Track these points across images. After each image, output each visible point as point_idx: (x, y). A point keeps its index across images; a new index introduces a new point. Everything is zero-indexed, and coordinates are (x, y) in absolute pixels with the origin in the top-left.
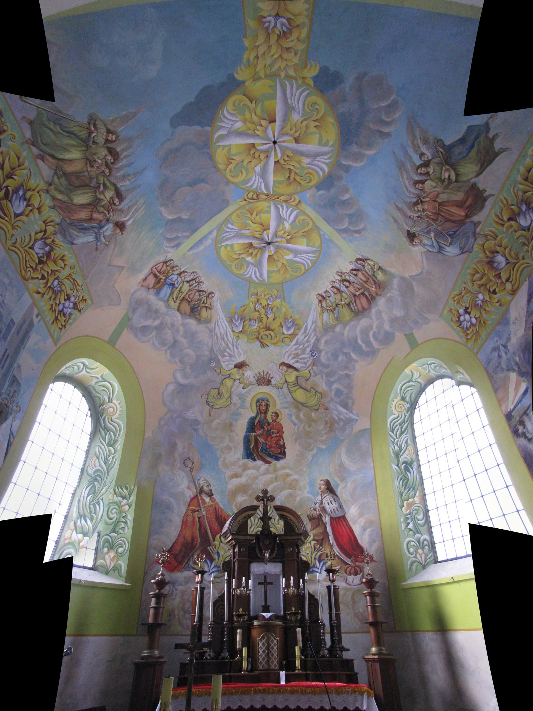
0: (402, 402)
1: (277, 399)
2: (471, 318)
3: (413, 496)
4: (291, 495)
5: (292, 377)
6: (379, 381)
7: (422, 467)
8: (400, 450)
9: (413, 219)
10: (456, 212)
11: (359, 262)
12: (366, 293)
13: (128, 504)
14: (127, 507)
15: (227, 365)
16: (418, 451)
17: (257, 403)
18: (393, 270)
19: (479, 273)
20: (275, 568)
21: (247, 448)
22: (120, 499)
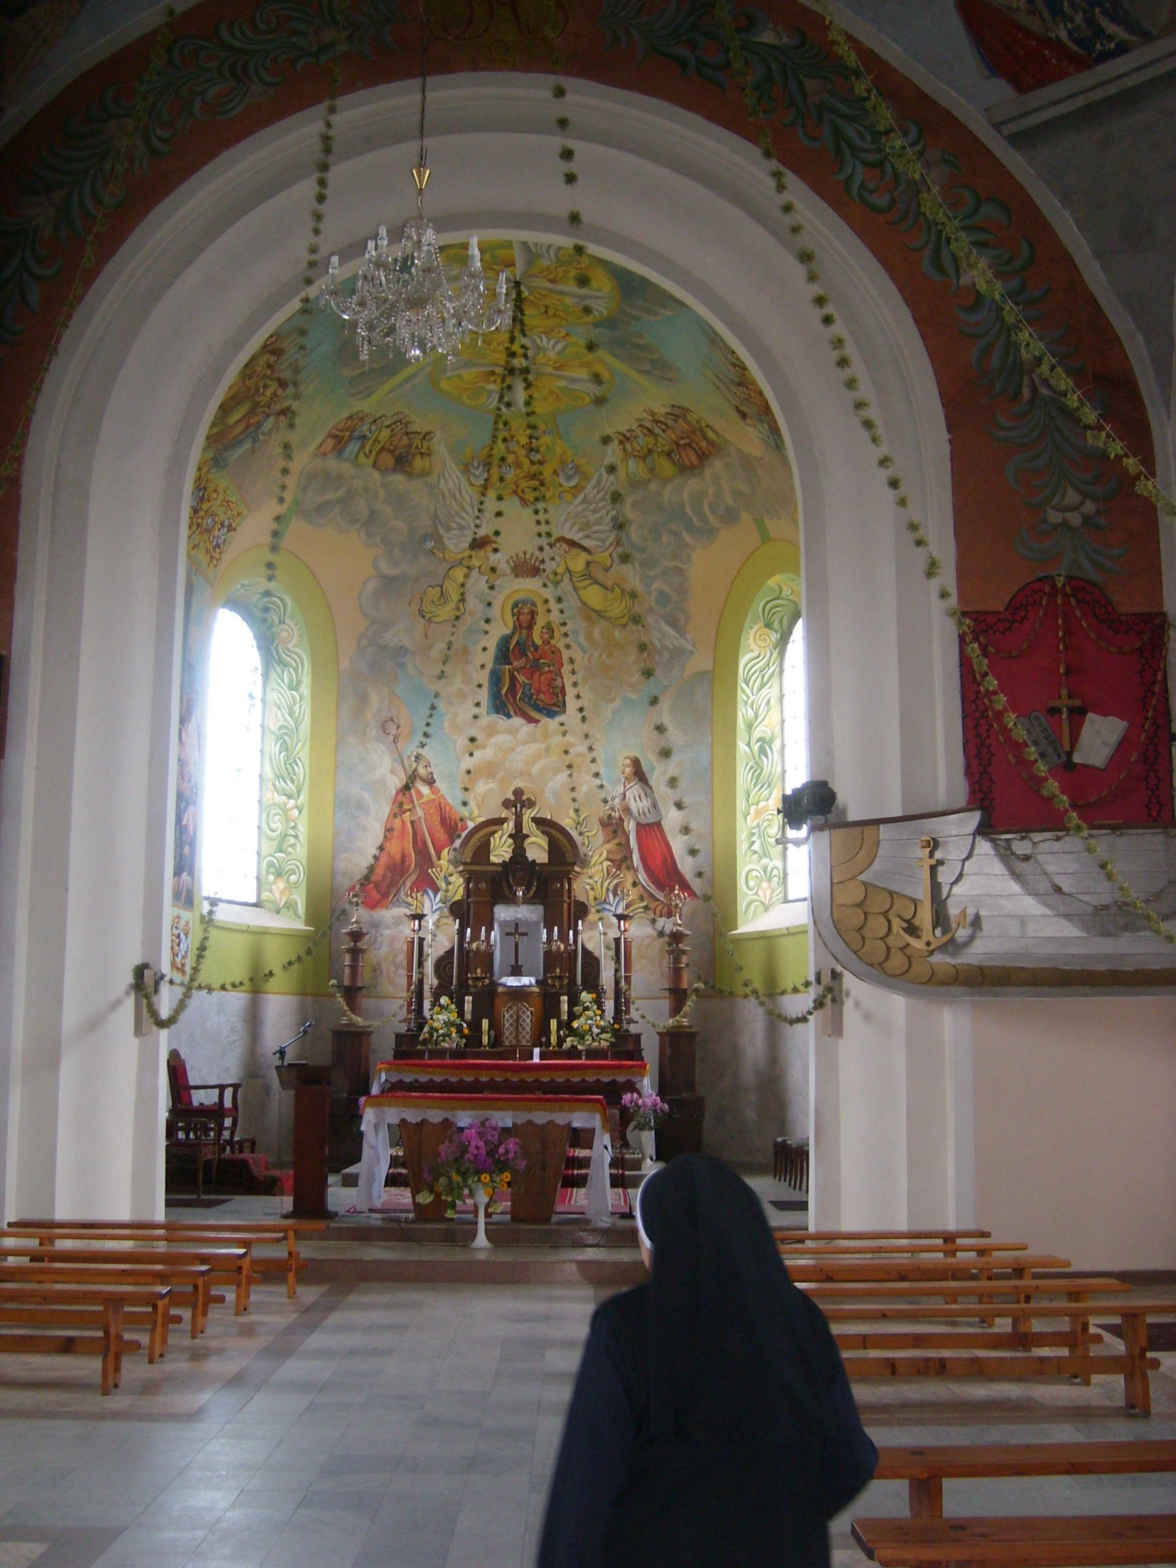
0: (767, 630)
8: (756, 717)
12: (694, 445)
13: (297, 807)
14: (296, 812)
17: (513, 609)
20: (527, 913)
21: (495, 695)
22: (284, 798)
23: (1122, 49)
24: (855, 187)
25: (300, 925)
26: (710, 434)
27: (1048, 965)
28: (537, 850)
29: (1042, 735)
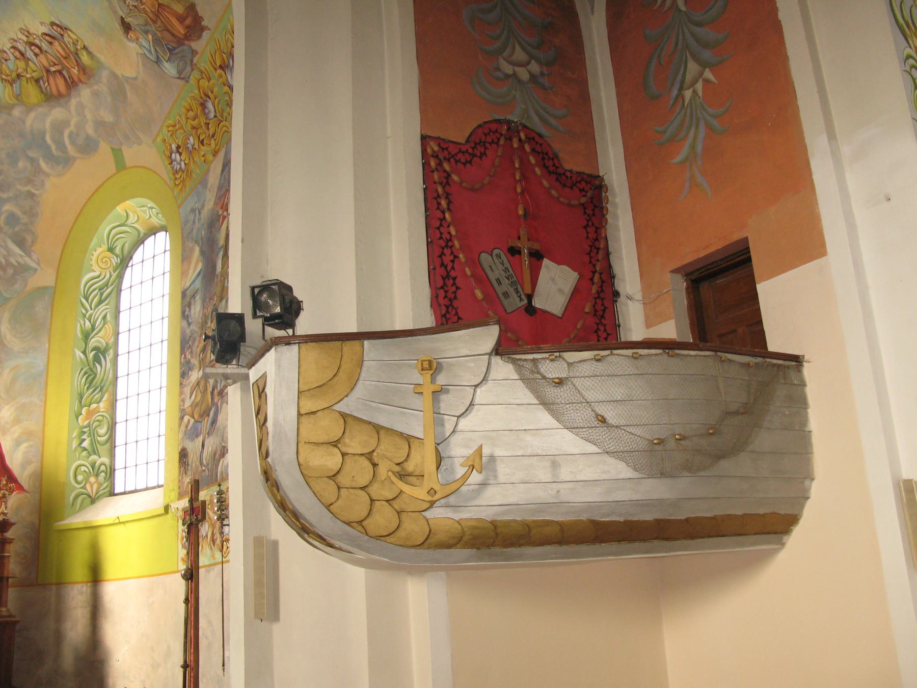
0: (109, 254)
2: (181, 160)
3: (99, 399)
6: (80, 214)
7: (119, 357)
8: (93, 328)
9: (128, 6)
10: (176, 25)
11: (55, 27)
12: (65, 73)
16: (118, 334)
18: (102, 58)
19: (193, 111)
26: (85, 58)
27: (584, 517)
29: (503, 273)
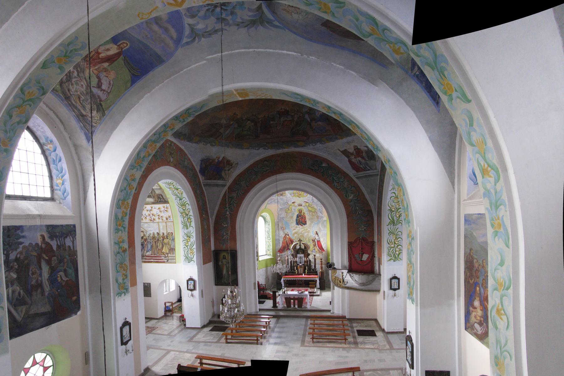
1: (304, 209)
4: (308, 234)
5: (307, 204)
15: (290, 203)
20: (302, 255)
23: (369, 170)
24: (335, 186)
25: (272, 257)
28: (303, 247)
